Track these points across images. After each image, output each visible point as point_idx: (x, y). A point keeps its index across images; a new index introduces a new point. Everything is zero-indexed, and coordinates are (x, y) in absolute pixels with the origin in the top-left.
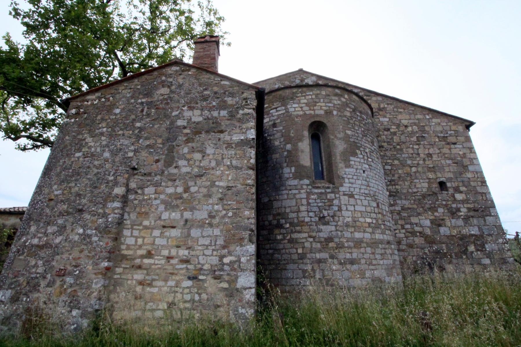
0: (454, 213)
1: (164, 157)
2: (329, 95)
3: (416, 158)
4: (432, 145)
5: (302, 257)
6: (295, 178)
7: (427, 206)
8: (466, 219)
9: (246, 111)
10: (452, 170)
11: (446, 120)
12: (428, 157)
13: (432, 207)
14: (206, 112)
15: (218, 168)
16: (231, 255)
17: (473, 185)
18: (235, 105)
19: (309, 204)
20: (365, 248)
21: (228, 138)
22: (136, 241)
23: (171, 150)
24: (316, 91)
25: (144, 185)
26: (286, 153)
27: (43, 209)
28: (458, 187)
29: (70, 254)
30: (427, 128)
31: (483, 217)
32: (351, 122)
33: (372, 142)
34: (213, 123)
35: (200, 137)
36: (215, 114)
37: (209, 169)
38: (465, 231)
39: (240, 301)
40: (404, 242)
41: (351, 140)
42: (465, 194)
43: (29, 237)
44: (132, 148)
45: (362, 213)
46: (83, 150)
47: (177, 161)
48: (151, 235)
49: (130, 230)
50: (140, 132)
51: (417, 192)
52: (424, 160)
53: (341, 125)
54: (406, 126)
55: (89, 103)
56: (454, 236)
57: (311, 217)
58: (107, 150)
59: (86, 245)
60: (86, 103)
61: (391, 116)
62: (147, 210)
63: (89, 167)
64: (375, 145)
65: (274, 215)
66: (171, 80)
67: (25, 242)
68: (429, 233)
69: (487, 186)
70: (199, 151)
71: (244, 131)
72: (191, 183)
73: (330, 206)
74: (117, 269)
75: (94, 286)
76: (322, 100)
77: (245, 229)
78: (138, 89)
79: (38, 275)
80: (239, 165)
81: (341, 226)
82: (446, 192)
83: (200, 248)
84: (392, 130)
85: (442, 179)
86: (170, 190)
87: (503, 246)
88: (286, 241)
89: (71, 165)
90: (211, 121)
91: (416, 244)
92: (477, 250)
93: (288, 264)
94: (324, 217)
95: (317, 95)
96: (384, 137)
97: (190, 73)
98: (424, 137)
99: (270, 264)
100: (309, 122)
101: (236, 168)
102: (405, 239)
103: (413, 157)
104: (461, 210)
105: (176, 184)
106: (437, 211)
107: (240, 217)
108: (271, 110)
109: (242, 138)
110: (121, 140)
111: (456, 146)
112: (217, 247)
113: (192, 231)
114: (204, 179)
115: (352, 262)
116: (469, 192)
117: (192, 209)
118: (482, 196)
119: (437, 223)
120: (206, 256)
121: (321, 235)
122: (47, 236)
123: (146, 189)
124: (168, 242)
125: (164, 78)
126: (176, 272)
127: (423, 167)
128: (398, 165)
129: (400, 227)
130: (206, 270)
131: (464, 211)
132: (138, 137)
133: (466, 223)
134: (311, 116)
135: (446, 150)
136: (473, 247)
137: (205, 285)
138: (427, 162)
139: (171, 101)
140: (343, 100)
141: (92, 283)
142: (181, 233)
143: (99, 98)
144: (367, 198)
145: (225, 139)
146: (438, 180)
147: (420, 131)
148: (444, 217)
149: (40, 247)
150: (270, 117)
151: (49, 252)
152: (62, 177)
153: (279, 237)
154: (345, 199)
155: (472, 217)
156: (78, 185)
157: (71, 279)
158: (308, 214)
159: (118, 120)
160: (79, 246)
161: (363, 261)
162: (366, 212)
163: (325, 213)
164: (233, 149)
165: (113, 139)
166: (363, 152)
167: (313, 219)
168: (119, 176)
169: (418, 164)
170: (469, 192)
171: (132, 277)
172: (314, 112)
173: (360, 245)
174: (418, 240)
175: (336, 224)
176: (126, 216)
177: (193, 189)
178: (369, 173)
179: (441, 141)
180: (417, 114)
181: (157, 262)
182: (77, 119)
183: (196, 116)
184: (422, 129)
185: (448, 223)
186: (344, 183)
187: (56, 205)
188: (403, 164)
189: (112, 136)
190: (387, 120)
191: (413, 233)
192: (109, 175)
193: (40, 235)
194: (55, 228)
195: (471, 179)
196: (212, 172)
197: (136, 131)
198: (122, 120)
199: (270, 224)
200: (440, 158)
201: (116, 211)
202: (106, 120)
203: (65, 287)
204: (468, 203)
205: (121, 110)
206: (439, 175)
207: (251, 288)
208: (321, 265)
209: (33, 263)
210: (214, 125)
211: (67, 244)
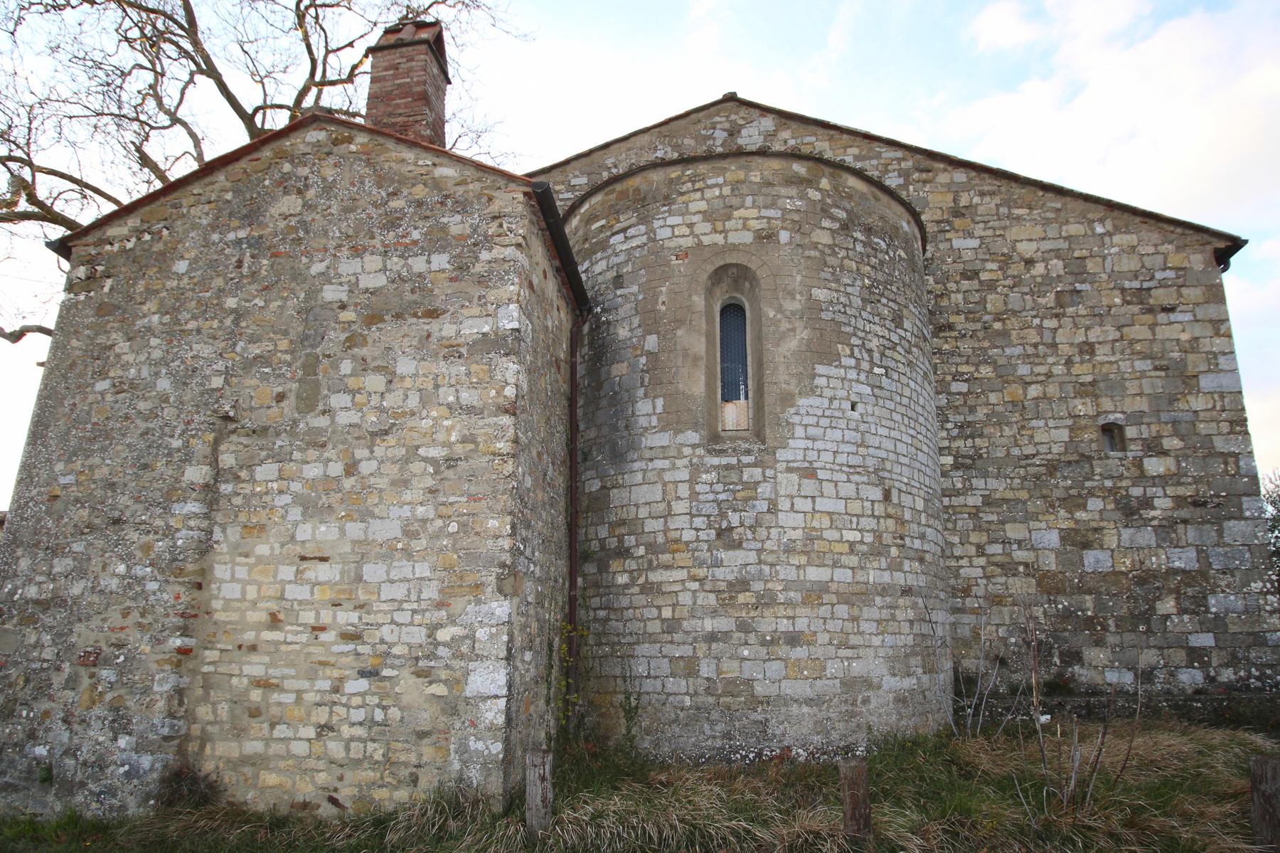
0: (1130, 511)
1: (295, 386)
3: (1045, 356)
4: (1099, 317)
5: (672, 626)
6: (663, 430)
7: (1058, 493)
8: (1167, 528)
9: (498, 252)
10: (1147, 390)
11: (1155, 237)
12: (1081, 352)
13: (1071, 496)
14: (395, 259)
15: (424, 413)
16: (454, 623)
17: (1204, 432)
18: (470, 237)
19: (694, 495)
20: (833, 605)
21: (449, 330)
22: (244, 592)
23: (311, 367)
24: (734, 171)
25: (252, 457)
26: (643, 360)
27: (39, 521)
28: (1159, 437)
29: (104, 620)
30: (1091, 266)
31: (1218, 521)
32: (831, 260)
33: (898, 321)
34: (413, 291)
35: (380, 330)
36: (418, 264)
37: (404, 414)
38: (1155, 562)
39: (473, 725)
40: (979, 591)
41: (823, 315)
42: (1177, 457)
43: (19, 583)
44: (220, 365)
45: (835, 517)
46: (112, 374)
47: (327, 396)
48: (275, 576)
49: (229, 566)
50: (236, 322)
51: (1034, 456)
52: (1069, 362)
53: (799, 272)
54: (1029, 262)
55: (116, 247)
56: (1122, 573)
57: (697, 530)
58: (164, 371)
59: (134, 599)
60: (108, 247)
61: (989, 232)
62: (264, 521)
63: (127, 417)
64: (907, 324)
65: (613, 526)
66: (304, 171)
67: (13, 593)
68: (1053, 567)
69: (1247, 433)
70: (378, 369)
71: (491, 308)
72: (361, 453)
74: (207, 653)
75: (156, 688)
76: (749, 200)
77: (490, 562)
78: (228, 201)
79: (45, 665)
80: (475, 403)
81: (772, 552)
82: (1120, 454)
83: (385, 607)
84: (984, 276)
85: (1111, 418)
86: (313, 471)
87: (1261, 602)
88: (636, 590)
89: (88, 413)
90: (408, 286)
91: (1011, 596)
92: (1182, 611)
93: (638, 643)
94: (730, 529)
95: (736, 185)
96: (960, 296)
97: (353, 148)
98: (1079, 292)
99: (600, 644)
101: (470, 410)
102: (984, 581)
103: (1037, 356)
104: (1157, 502)
105: (326, 455)
106: (1084, 507)
107: (477, 533)
108: (613, 234)
109: (486, 329)
110: (195, 346)
111: (1173, 317)
112: (424, 605)
113: (365, 568)
114: (391, 439)
115: (794, 639)
116: (1189, 452)
117: (366, 516)
118: (1226, 464)
119: (1079, 540)
120: (398, 624)
121: (719, 573)
122: (54, 580)
123: (258, 469)
124: (312, 593)
125: (287, 167)
126: (332, 659)
127: (1061, 384)
128: (989, 379)
129: (973, 550)
130: (399, 657)
131: (1163, 504)
132: (233, 336)
133: (1164, 540)
135: (1139, 332)
136: (1172, 603)
137: (397, 689)
138: (1076, 370)
139: (307, 232)
140: (814, 195)
141: (153, 680)
142: (342, 573)
143: (138, 232)
144: (855, 478)
145: (444, 334)
146: (1101, 421)
147: (1071, 273)
148: (1104, 524)
149: (44, 605)
150: (608, 257)
151: (61, 615)
152: (72, 444)
153: (622, 579)
155: (1185, 522)
156: (108, 462)
157: (111, 672)
158: (691, 523)
159: (182, 291)
160: (121, 603)
161: (823, 638)
163: (734, 519)
164: (461, 361)
165: (175, 343)
166: (856, 350)
167: (702, 535)
168: (193, 436)
169: (1049, 375)
170: (1189, 452)
171: (241, 669)
172: (725, 238)
173: (820, 597)
174: (1021, 586)
175: (759, 545)
176: (217, 535)
177: (366, 468)
178: (870, 408)
179: (1129, 303)
180: (1067, 222)
181: (290, 638)
182: (92, 294)
183: (371, 273)
184: (1077, 270)
185: (1111, 540)
187: (66, 509)
188: (1004, 376)
189: (174, 333)
190: (974, 243)
191: (1009, 568)
192: (172, 436)
193: (39, 578)
194: (69, 562)
195: (1202, 414)
196: (411, 423)
197: (228, 322)
198: (193, 290)
199: (603, 548)
200: (1118, 356)
201: (192, 523)
202: (157, 292)
203: (100, 689)
204: (1179, 484)
205: (190, 264)
206: (1107, 404)
207: (496, 697)
208: (714, 646)
209: (33, 639)
210: (415, 297)
211: (96, 598)
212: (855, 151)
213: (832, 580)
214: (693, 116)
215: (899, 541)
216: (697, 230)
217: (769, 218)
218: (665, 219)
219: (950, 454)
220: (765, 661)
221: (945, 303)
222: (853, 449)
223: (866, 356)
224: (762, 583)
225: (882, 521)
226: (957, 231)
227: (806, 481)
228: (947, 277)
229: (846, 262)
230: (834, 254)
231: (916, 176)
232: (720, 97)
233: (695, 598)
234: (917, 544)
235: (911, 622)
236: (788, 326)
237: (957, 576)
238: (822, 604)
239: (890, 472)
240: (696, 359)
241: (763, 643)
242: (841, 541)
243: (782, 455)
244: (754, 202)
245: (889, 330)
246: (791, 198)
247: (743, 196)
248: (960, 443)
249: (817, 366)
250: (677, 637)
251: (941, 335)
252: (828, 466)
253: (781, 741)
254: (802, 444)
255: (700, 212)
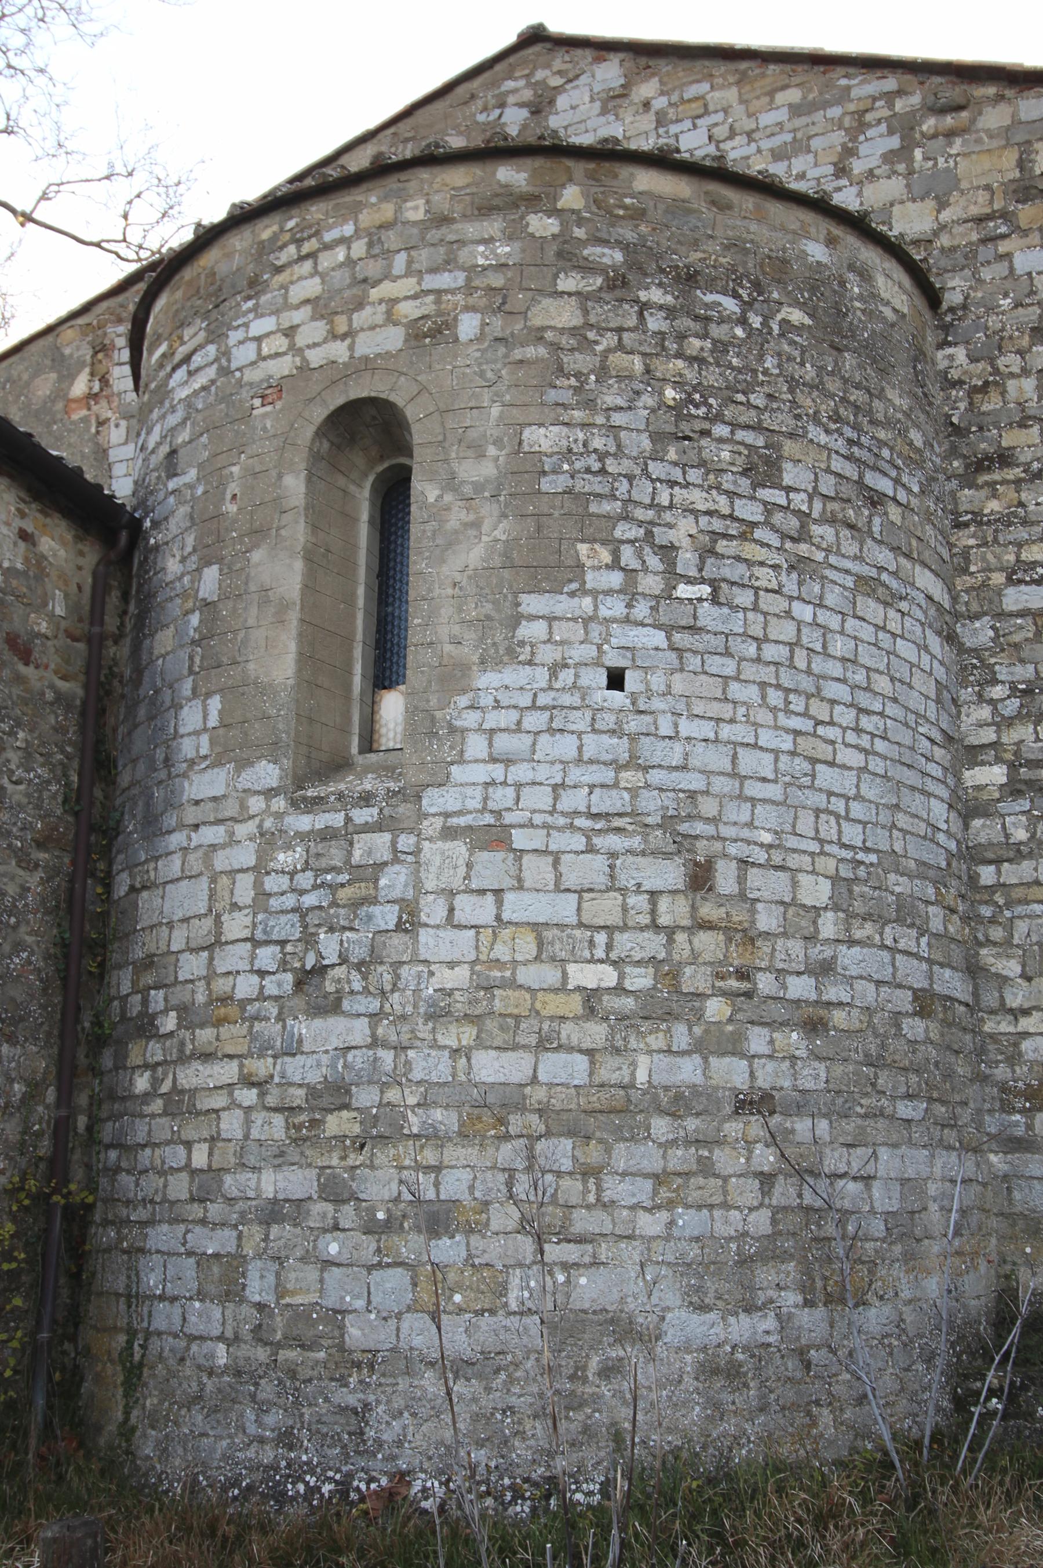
2: (443, 220)
26: (195, 619)
33: (762, 469)
45: (549, 934)
57: (262, 974)
73: (356, 904)
95: (374, 236)
100: (319, 414)
121: (296, 1068)
134: (337, 373)
144: (614, 842)
154: (445, 857)
158: (253, 957)
162: (581, 925)
163: (329, 946)
172: (351, 348)
173: (502, 1121)
175: (374, 1005)
186: (461, 761)
208: (275, 1230)
212: (793, 95)
213: (534, 1080)
214: (461, 90)
215: (733, 983)
216: (301, 339)
217: (438, 292)
218: (246, 325)
219: (999, 760)
220: (370, 1268)
221: (991, 404)
222: (607, 775)
223: (654, 562)
224: (375, 1090)
225: (681, 937)
226: (1025, 233)
227: (484, 856)
228: (999, 343)
229: (617, 360)
230: (585, 345)
231: (929, 124)
232: (510, 38)
233: (248, 1123)
234: (800, 987)
235: (766, 1180)
236: (463, 515)
237: (1014, 1058)
238: (507, 1137)
239: (714, 821)
240: (284, 606)
241: (371, 1228)
242: (562, 989)
243: (434, 801)
244: (410, 262)
245: (731, 495)
246: (487, 241)
247: (388, 254)
248: (1024, 732)
249: (524, 598)
250: (215, 1210)
251: (983, 478)
252: (538, 819)
253: (393, 1458)
254: (480, 773)
255: (307, 301)
